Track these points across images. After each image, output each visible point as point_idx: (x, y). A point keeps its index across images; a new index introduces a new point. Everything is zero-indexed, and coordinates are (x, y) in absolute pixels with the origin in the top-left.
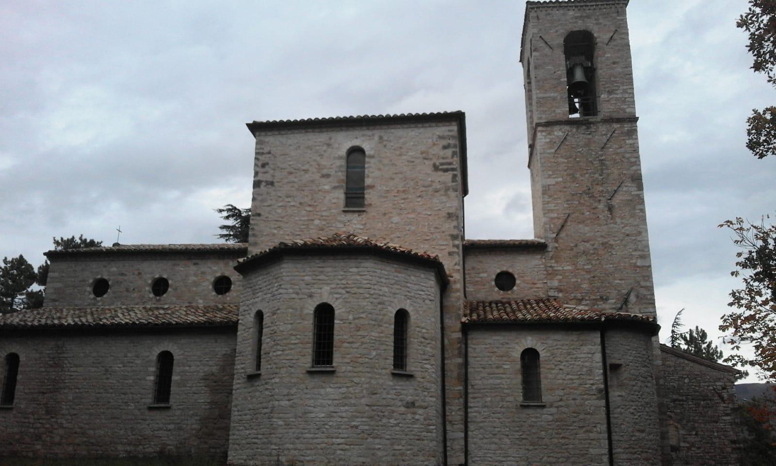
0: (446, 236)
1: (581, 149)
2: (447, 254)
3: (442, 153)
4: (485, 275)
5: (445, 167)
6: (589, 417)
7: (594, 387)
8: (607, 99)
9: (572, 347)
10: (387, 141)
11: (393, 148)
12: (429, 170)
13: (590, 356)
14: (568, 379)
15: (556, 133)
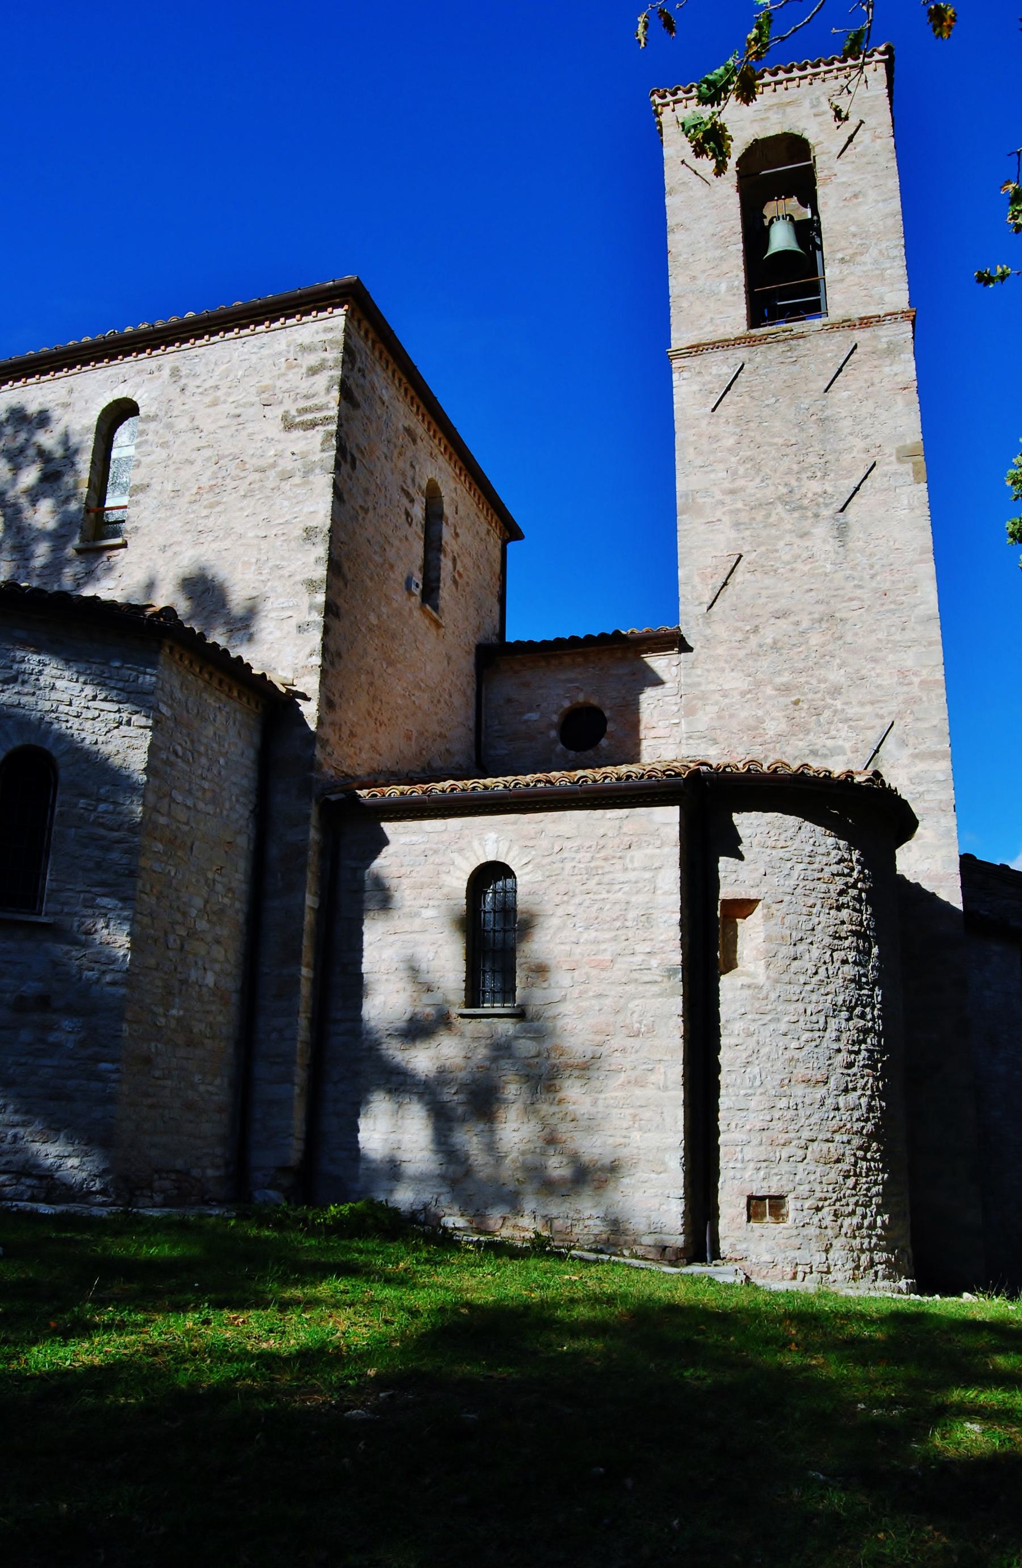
0: (295, 583)
1: (773, 400)
2: (294, 631)
3: (304, 385)
4: (533, 716)
5: (309, 417)
6: (636, 1042)
7: (654, 962)
8: (839, 278)
9: (602, 854)
10: (187, 376)
11: (200, 390)
12: (273, 428)
13: (648, 875)
14: (587, 942)
15: (714, 370)
